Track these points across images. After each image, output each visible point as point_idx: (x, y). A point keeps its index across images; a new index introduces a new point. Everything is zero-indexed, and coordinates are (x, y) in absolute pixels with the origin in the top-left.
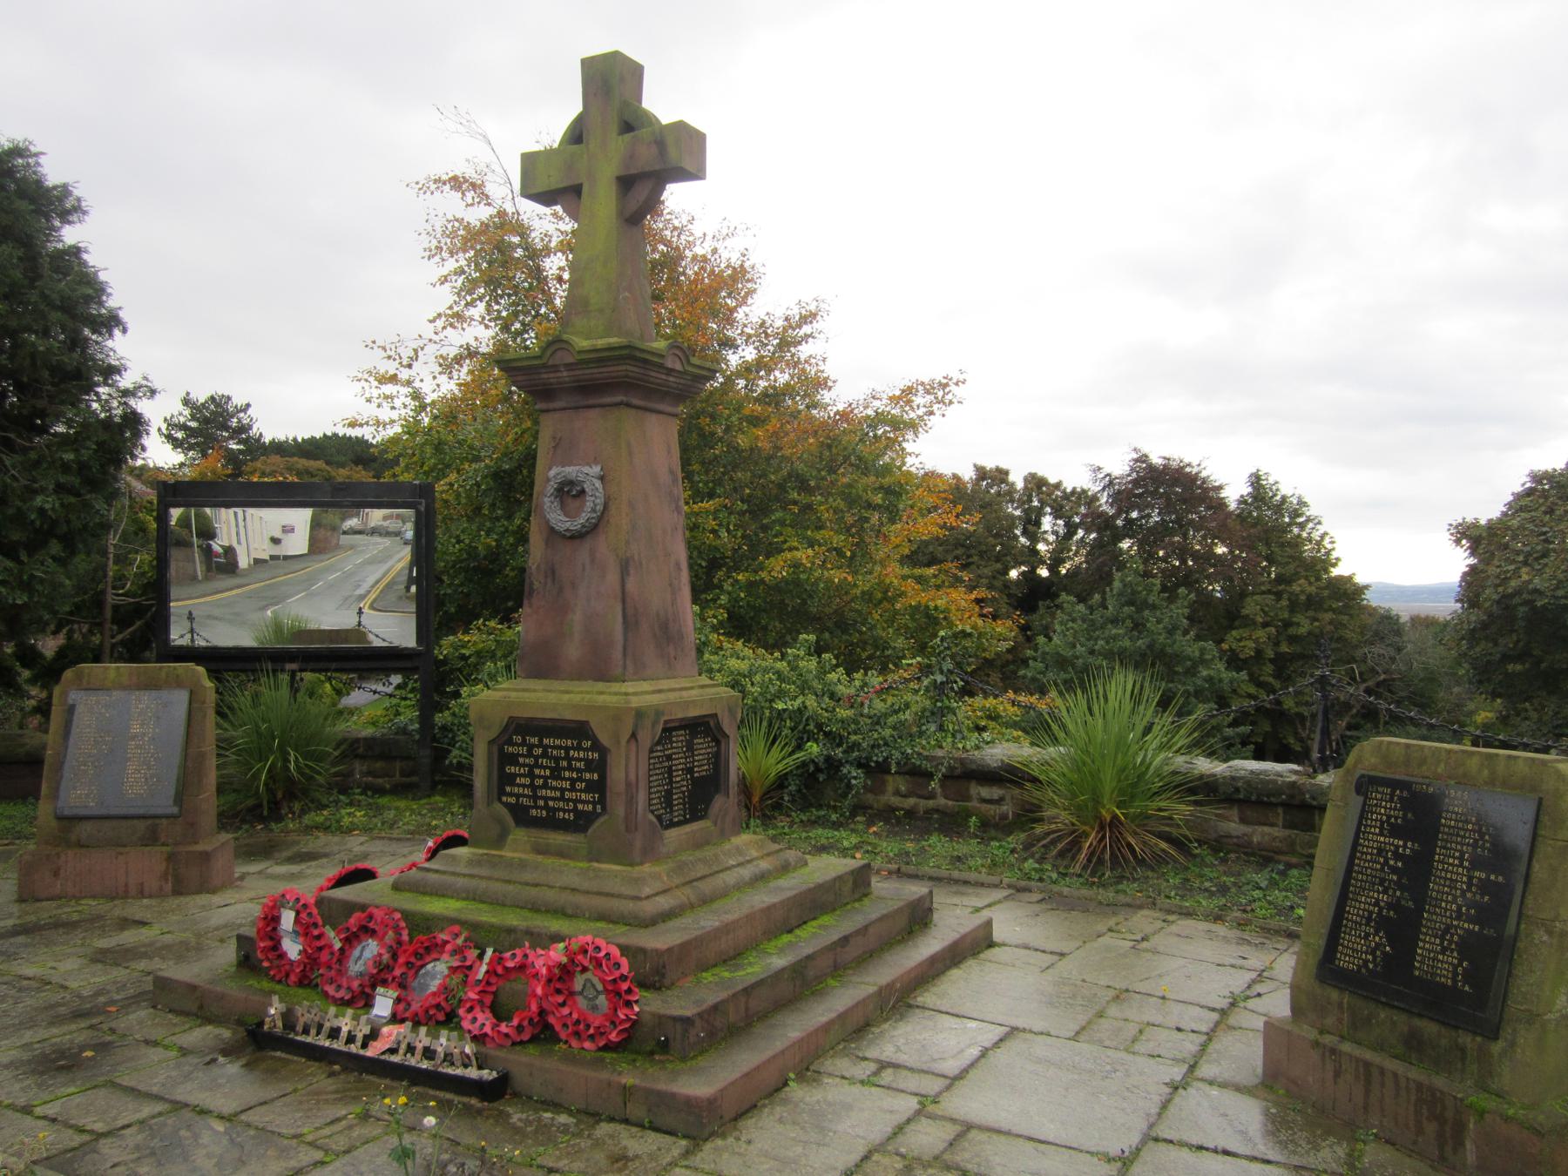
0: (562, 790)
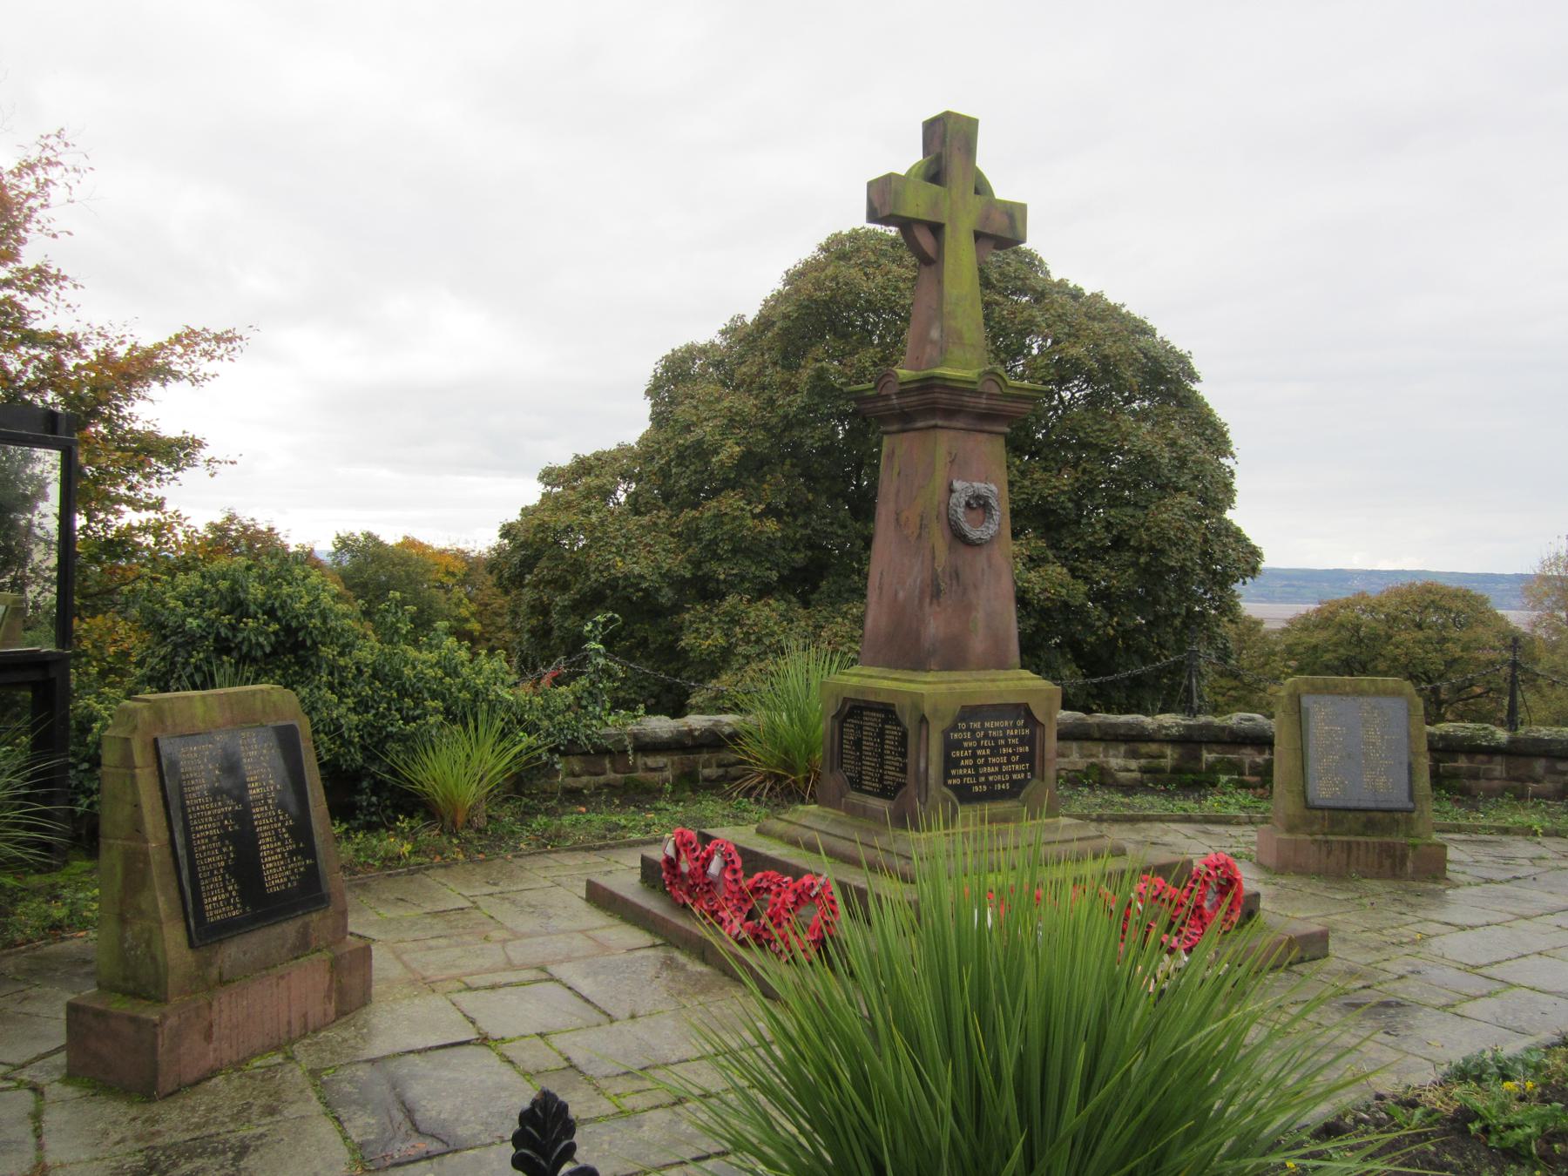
0: (1000, 765)
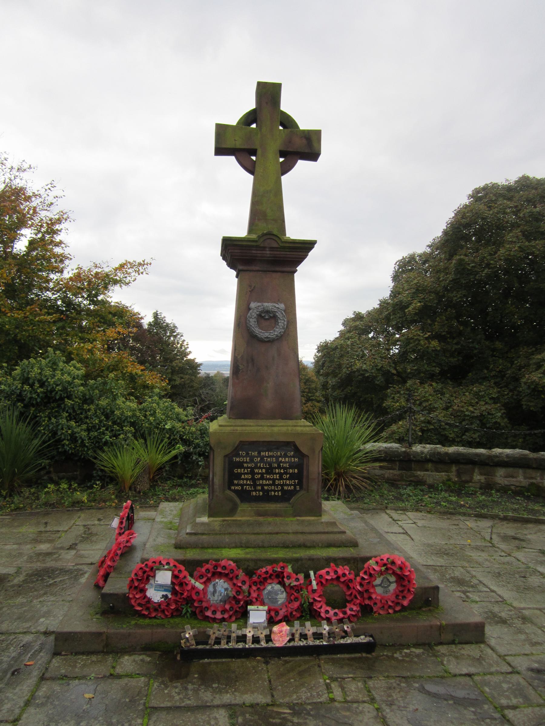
0: (274, 480)
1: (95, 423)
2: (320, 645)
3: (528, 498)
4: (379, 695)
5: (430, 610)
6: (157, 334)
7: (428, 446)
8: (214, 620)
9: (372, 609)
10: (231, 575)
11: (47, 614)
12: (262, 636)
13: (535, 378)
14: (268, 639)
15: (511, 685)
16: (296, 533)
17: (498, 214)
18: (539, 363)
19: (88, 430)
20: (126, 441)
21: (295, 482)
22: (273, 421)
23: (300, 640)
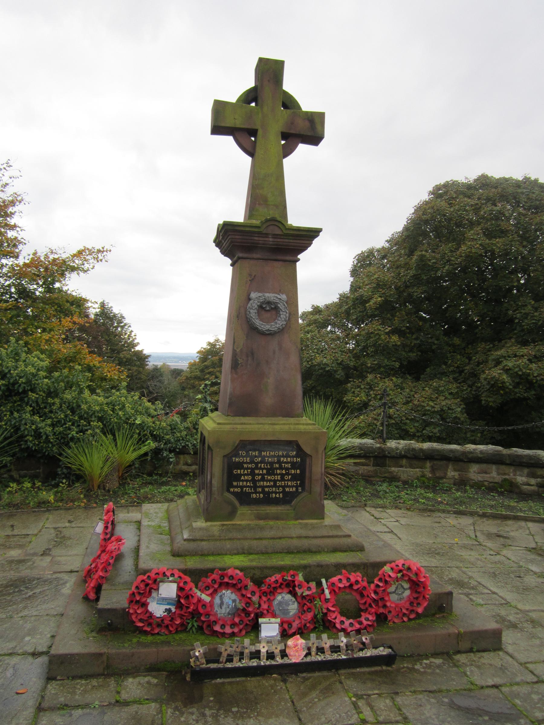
0: (275, 481)
1: (61, 418)
2: (339, 660)
3: (501, 494)
4: (410, 713)
5: (443, 617)
6: (103, 324)
7: (402, 442)
8: (223, 635)
9: (386, 618)
10: (239, 586)
11: (32, 632)
12: (277, 652)
13: (495, 374)
14: (284, 654)
15: (540, 696)
16: (299, 537)
17: (459, 211)
18: (498, 359)
19: (53, 425)
20: (94, 436)
21: (297, 483)
22: (273, 418)
23: (317, 654)
